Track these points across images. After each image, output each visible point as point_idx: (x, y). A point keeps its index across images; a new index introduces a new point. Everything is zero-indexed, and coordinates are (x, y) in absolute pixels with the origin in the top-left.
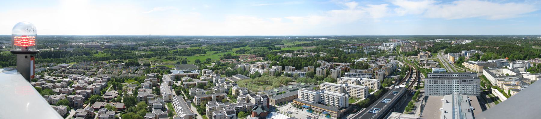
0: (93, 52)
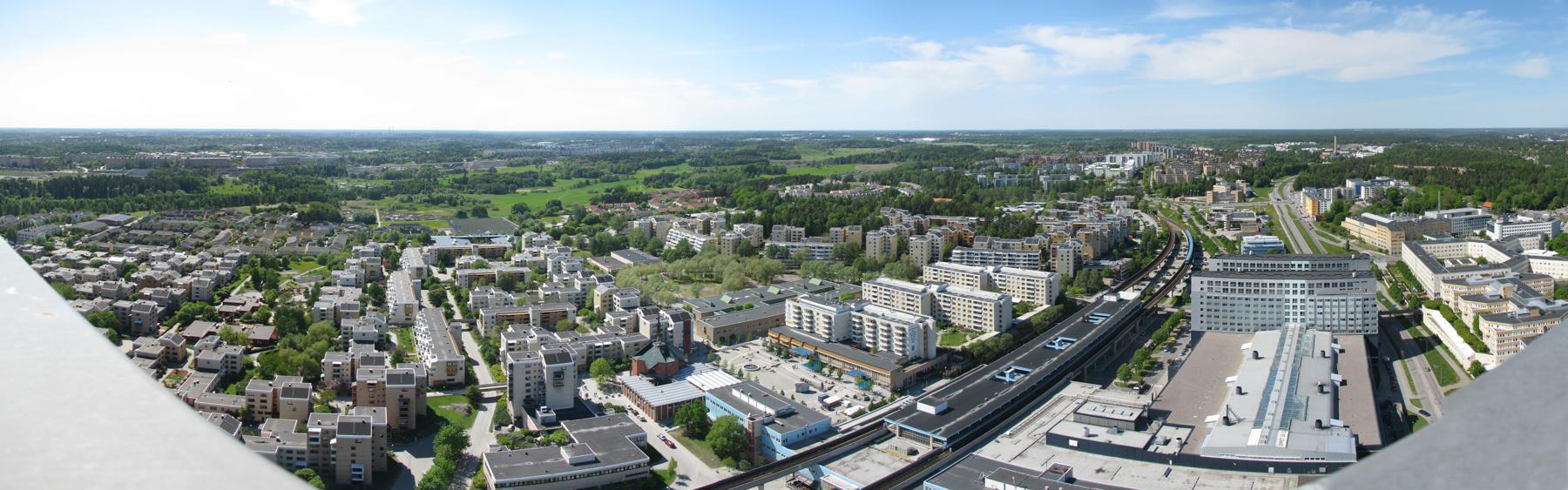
0: (210, 180)
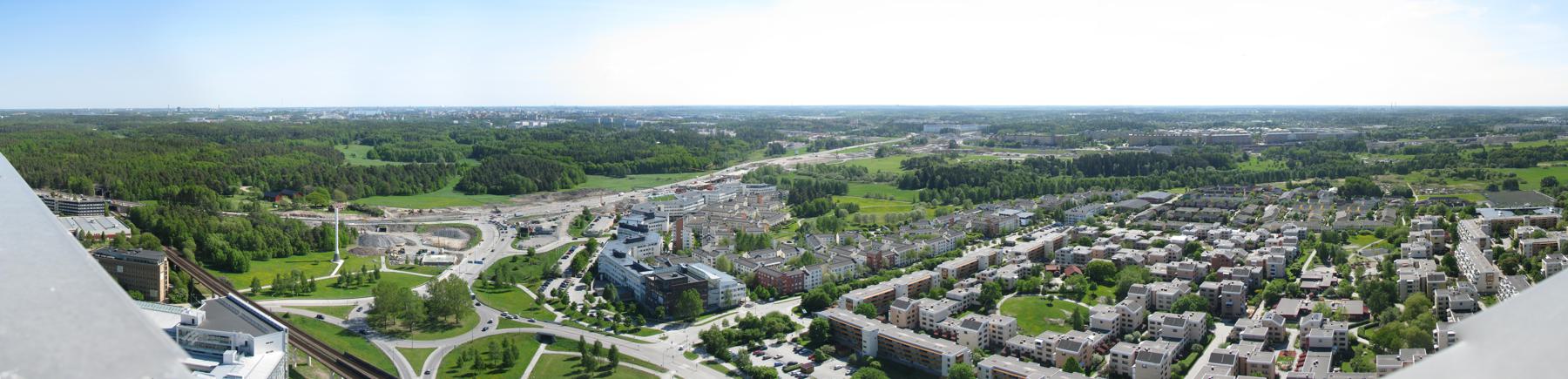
0: (1236, 155)
